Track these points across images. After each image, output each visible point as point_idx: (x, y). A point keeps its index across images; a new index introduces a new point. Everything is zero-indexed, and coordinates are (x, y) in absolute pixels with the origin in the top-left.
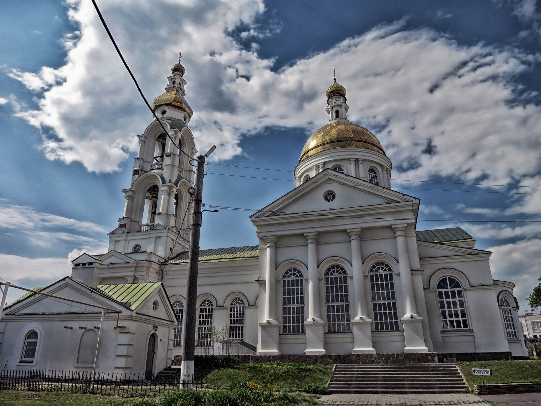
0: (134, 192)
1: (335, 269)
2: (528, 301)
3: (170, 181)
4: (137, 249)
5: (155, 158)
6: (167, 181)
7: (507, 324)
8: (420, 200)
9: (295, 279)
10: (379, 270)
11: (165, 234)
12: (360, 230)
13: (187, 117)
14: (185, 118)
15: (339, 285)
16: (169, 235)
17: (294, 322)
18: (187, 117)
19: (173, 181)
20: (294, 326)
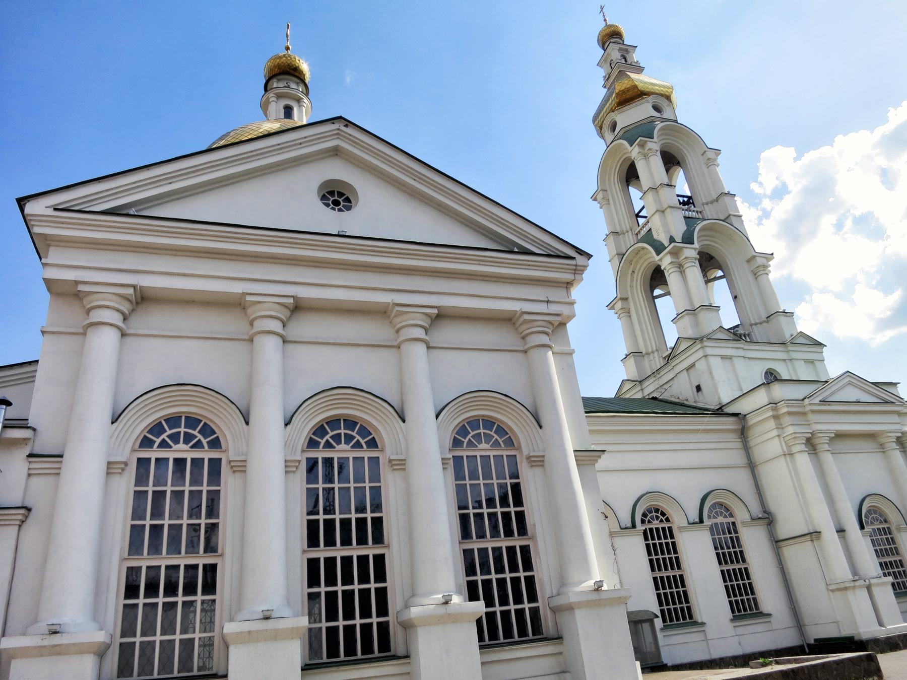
0: (624, 299)
1: (342, 431)
2: (777, 182)
3: (672, 240)
4: (772, 377)
5: (637, 216)
6: (666, 242)
7: (736, 601)
8: (21, 202)
9: (492, 454)
10: (177, 442)
11: (700, 354)
12: (291, 301)
13: (663, 102)
14: (657, 108)
15: (166, 522)
16: (709, 351)
17: (349, 615)
18: (663, 102)
19: (678, 238)
20: (367, 628)
